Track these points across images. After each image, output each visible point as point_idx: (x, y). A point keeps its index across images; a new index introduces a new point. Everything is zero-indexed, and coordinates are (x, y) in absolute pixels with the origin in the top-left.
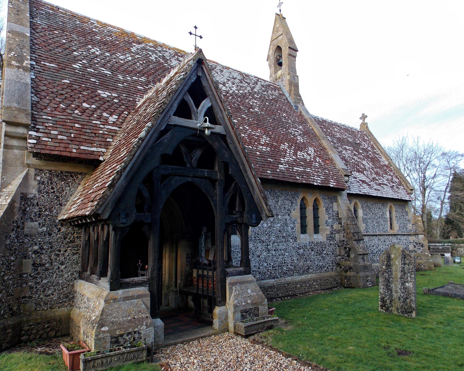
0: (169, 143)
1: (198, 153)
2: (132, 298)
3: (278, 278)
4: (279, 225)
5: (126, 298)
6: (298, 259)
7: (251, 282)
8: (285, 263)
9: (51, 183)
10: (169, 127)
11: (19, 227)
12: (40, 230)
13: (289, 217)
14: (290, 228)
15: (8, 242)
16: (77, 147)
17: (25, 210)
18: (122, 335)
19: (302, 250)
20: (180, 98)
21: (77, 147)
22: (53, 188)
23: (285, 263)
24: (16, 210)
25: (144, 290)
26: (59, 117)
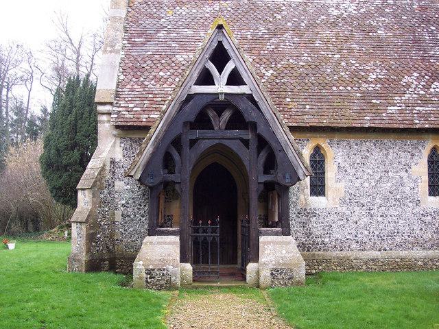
0: (191, 112)
1: (227, 115)
2: (165, 243)
3: (385, 250)
4: (389, 184)
5: (159, 243)
6: (421, 229)
7: (289, 243)
8: (398, 233)
9: (132, 149)
10: (190, 97)
11: (110, 185)
12: (125, 188)
13: (407, 174)
14: (408, 189)
15: (102, 196)
16: (147, 116)
17: (114, 172)
18: (153, 270)
19: (429, 218)
20: (200, 67)
21: (147, 116)
22: (133, 153)
23: (398, 233)
24: (107, 172)
25: (177, 239)
26: (137, 90)
